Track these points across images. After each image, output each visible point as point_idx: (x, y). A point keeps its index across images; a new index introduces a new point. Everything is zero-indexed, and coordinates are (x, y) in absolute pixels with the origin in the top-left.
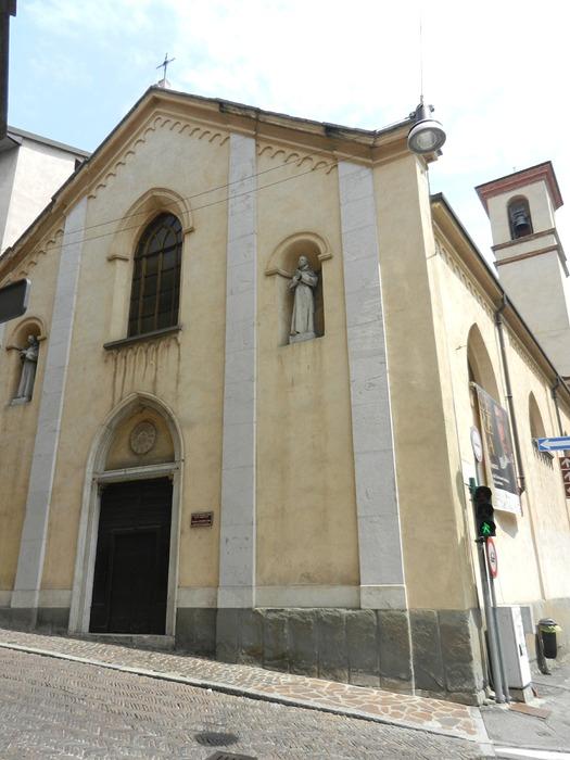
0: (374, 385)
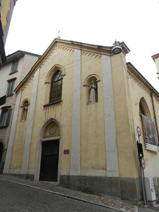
0: (110, 115)
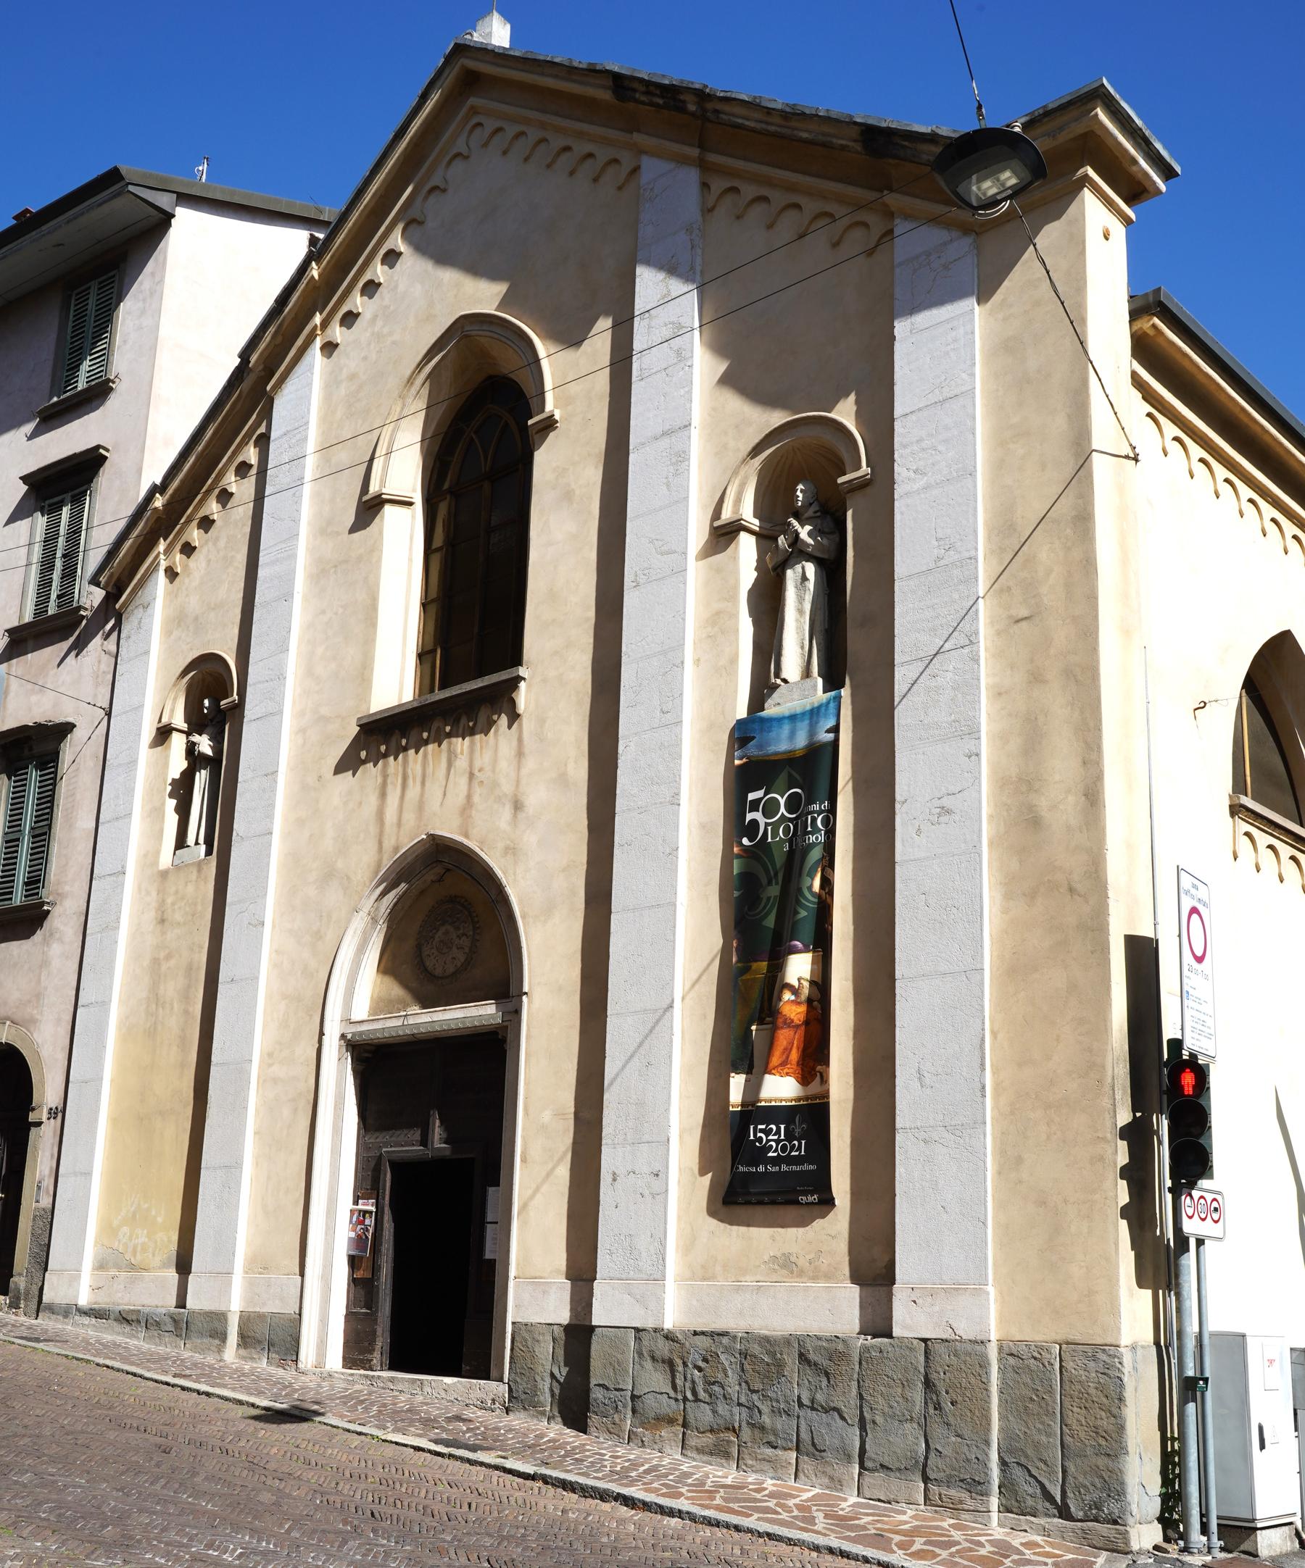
0: (949, 812)
